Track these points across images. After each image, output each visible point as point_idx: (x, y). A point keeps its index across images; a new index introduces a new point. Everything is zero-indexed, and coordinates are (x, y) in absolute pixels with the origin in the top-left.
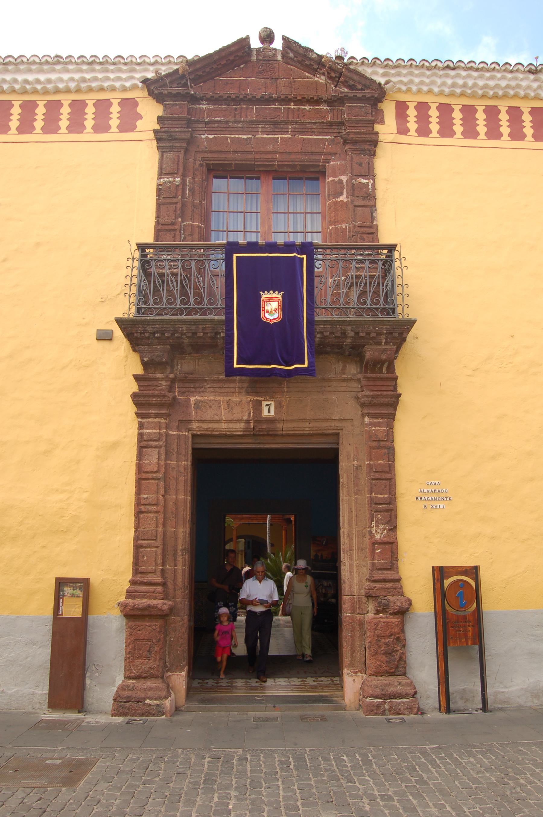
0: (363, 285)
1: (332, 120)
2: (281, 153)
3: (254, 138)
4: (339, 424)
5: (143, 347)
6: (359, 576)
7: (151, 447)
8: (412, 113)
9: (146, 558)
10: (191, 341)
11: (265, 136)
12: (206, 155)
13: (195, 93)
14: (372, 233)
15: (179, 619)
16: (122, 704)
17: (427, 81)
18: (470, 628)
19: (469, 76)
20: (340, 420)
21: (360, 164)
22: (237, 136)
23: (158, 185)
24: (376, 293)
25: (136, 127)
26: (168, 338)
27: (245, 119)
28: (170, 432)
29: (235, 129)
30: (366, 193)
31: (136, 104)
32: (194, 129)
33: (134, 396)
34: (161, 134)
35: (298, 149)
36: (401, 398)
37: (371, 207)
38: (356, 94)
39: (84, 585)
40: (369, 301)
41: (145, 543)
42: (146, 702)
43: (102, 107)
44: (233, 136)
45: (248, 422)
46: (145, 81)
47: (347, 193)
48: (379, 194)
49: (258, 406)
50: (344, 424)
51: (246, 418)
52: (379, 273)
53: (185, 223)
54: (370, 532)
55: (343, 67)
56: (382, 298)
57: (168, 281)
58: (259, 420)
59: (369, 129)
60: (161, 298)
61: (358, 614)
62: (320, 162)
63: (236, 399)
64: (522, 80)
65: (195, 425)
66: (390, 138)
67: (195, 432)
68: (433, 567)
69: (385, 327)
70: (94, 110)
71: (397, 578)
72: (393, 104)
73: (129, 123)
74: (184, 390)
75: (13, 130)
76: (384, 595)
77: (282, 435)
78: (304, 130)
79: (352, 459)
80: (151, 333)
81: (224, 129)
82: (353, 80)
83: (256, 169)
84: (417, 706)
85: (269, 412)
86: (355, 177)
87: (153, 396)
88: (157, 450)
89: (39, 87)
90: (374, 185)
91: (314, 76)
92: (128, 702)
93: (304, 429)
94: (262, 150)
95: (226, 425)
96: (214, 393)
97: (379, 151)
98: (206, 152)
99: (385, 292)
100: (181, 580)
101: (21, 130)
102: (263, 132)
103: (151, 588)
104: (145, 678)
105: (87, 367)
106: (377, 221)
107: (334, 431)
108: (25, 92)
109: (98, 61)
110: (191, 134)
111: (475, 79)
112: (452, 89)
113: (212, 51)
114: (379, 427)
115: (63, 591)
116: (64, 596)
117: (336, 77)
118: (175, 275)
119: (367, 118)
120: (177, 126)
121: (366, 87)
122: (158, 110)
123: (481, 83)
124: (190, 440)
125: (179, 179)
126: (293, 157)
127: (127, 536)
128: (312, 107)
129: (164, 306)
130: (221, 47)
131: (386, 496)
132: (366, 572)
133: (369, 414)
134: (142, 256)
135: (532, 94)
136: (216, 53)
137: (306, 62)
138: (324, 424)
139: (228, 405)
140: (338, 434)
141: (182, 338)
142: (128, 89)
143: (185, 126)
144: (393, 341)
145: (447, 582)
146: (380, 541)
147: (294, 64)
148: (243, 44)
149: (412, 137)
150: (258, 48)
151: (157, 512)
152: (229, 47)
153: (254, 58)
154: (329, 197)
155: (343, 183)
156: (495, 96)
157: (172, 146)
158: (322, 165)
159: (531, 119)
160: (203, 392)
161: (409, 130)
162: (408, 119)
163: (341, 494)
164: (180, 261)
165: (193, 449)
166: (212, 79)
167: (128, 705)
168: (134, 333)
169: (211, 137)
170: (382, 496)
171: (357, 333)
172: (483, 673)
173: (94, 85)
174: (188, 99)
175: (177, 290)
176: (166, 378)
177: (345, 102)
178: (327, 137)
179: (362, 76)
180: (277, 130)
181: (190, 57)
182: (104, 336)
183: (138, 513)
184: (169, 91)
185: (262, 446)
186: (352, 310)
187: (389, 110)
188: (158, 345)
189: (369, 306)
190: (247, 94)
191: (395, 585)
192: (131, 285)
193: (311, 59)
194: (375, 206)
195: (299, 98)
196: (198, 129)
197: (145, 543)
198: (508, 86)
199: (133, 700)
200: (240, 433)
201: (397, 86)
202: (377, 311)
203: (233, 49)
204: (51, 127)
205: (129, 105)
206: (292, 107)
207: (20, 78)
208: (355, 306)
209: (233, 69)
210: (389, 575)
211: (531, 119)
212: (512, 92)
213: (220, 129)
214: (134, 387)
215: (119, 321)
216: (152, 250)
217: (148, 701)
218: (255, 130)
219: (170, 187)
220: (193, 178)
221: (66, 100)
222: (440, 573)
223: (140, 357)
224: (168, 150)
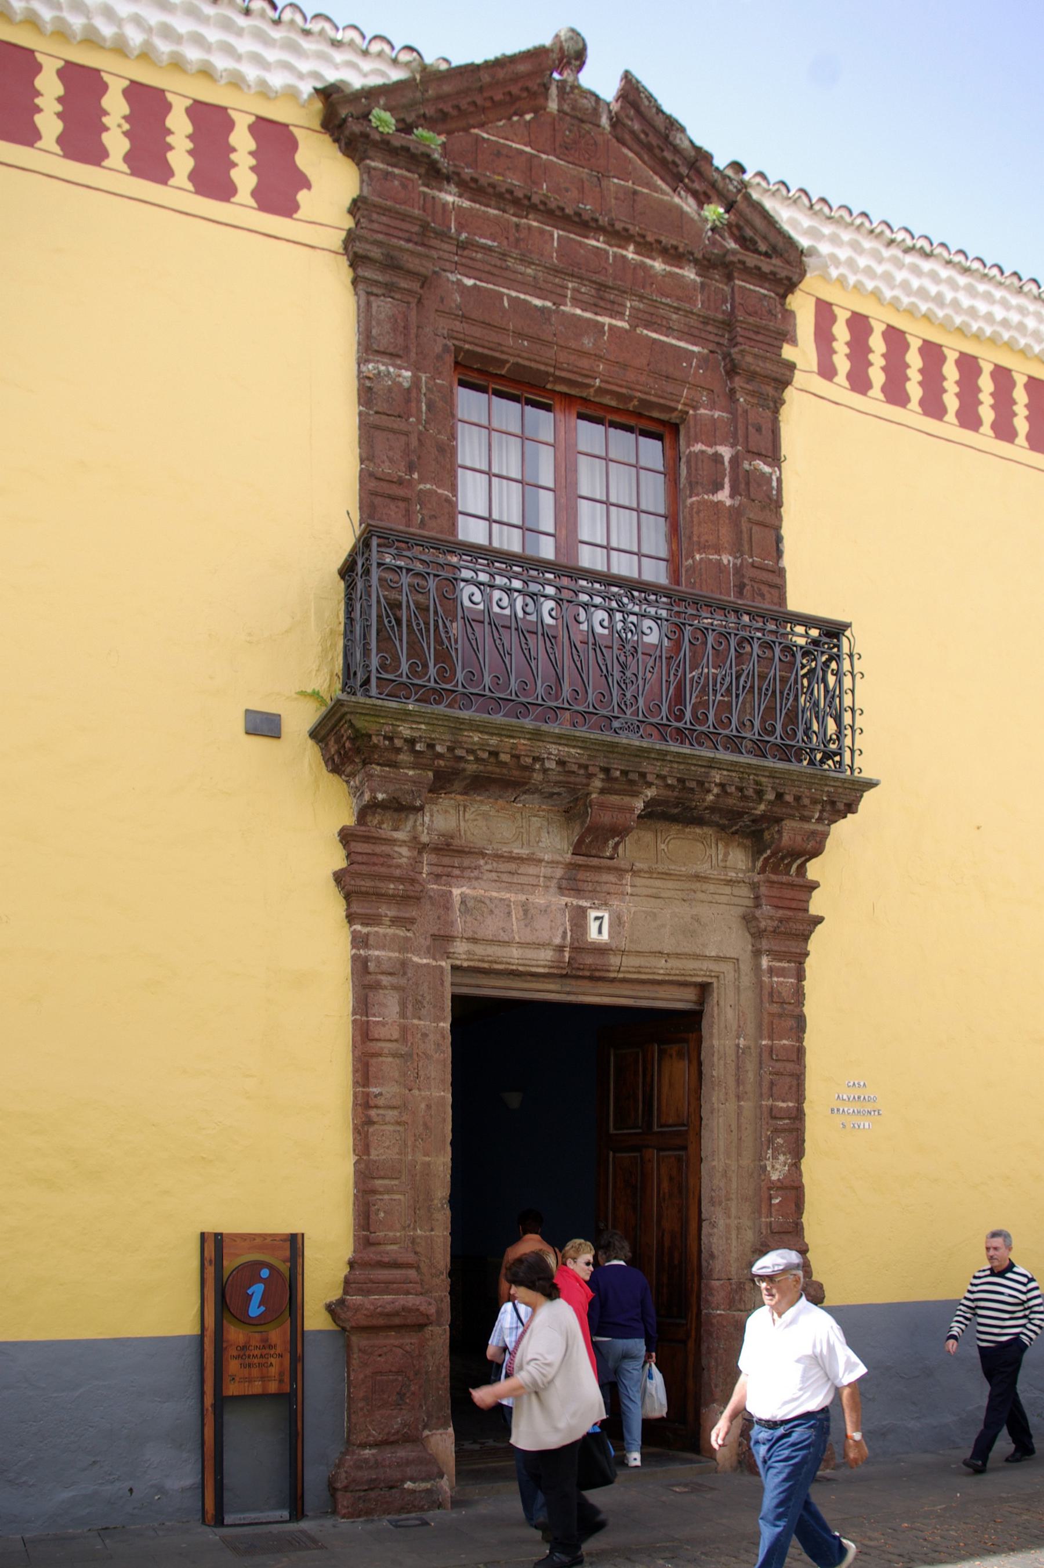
4: (715, 967)
5: (378, 768)
9: (382, 1215)
11: (578, 312)
16: (362, 1494)
20: (718, 959)
22: (522, 296)
28: (416, 959)
33: (339, 877)
42: (406, 1486)
45: (560, 949)
49: (579, 918)
51: (557, 941)
56: (689, 708)
58: (580, 947)
63: (539, 899)
67: (458, 963)
69: (826, 789)
73: (280, 191)
74: (439, 870)
79: (734, 1033)
80: (406, 740)
82: (753, 227)
83: (549, 386)
85: (600, 932)
91: (674, 190)
92: (372, 1489)
93: (656, 970)
95: (520, 951)
102: (576, 302)
104: (392, 1443)
113: (479, 60)
120: (400, 234)
128: (668, 268)
131: (791, 1104)
133: (769, 952)
136: (488, 65)
138: (691, 965)
139: (526, 912)
141: (467, 761)
143: (415, 238)
146: (779, 1184)
147: (636, 147)
155: (723, 463)
157: (392, 284)
158: (681, 411)
160: (477, 878)
164: (404, 571)
165: (455, 998)
167: (372, 1494)
169: (470, 282)
170: (784, 1105)
171: (780, 796)
173: (193, 54)
174: (422, 171)
177: (736, 274)
178: (696, 349)
180: (602, 304)
182: (264, 726)
193: (676, 150)
199: (382, 1485)
213: (488, 268)
217: (408, 1485)
224: (379, 291)
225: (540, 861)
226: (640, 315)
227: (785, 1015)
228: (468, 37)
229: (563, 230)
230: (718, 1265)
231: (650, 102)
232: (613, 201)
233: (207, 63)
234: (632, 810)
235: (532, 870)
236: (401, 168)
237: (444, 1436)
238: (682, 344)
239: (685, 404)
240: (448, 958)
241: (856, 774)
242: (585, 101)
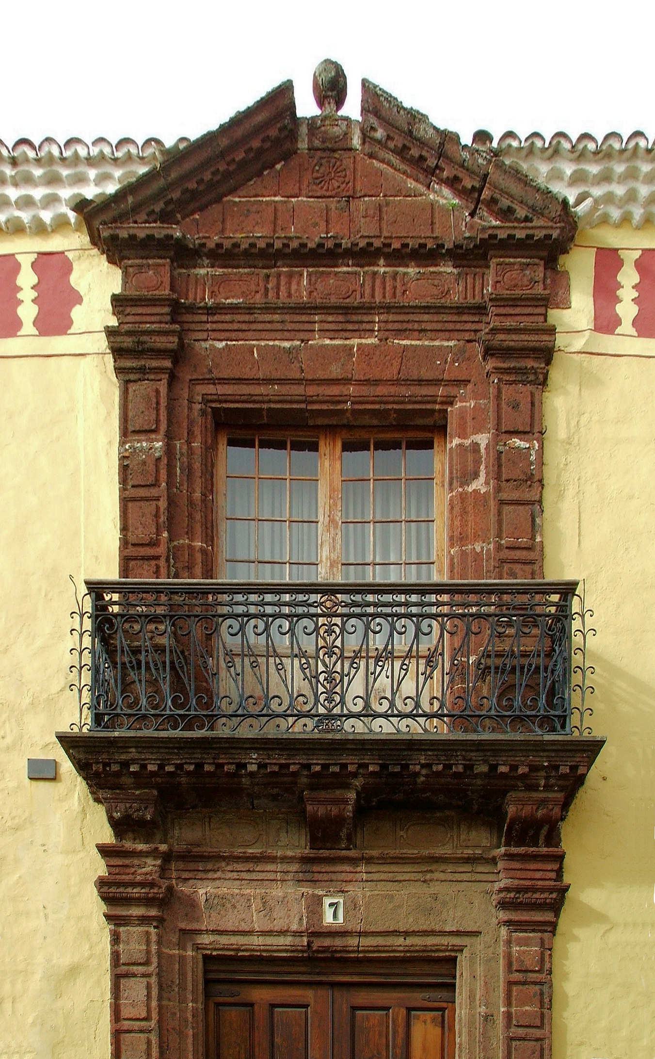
1: (461, 301)
3: (306, 348)
7: (134, 975)
10: (194, 780)
11: (328, 342)
13: (184, 236)
14: (531, 562)
20: (457, 933)
22: (271, 343)
23: (122, 458)
25: (71, 322)
26: (153, 774)
27: (287, 301)
30: (525, 473)
31: (67, 267)
32: (186, 326)
33: (102, 883)
35: (390, 373)
36: (569, 894)
37: (532, 503)
38: (512, 232)
44: (263, 343)
46: (81, 206)
47: (487, 474)
50: (465, 941)
53: (175, 543)
57: (147, 663)
59: (535, 318)
60: (163, 699)
63: (277, 892)
66: (578, 343)
67: (209, 952)
77: (357, 960)
81: (244, 327)
83: (311, 423)
86: (504, 436)
87: (134, 885)
88: (145, 980)
91: (428, 187)
94: (320, 375)
96: (238, 882)
97: (555, 374)
99: (549, 683)
105: (16, 829)
106: (542, 535)
110: (181, 339)
113: (214, 127)
114: (527, 945)
118: (160, 649)
119: (534, 292)
124: (201, 964)
125: (161, 443)
126: (381, 390)
129: (143, 712)
130: (232, 114)
136: (224, 129)
137: (412, 152)
142: (49, 229)
144: (560, 782)
150: (313, 118)
153: (303, 145)
154: (451, 484)
164: (168, 618)
168: (91, 764)
179: (524, 180)
182: (42, 772)
184: (132, 232)
186: (487, 721)
187: (580, 266)
188: (136, 789)
190: (290, 238)
193: (422, 143)
194: (540, 502)
196: (193, 326)
203: (260, 118)
205: (54, 267)
206: (382, 270)
208: (493, 712)
213: (236, 326)
214: (100, 868)
215: (66, 740)
216: (116, 597)
218: (307, 327)
219: (144, 463)
223: (107, 812)
225: (275, 858)
226: (390, 326)
228: (195, 108)
229: (310, 266)
231: (390, 102)
234: (345, 801)
235: (270, 867)
236: (153, 258)
238: (437, 343)
241: (585, 734)
242: (336, 129)
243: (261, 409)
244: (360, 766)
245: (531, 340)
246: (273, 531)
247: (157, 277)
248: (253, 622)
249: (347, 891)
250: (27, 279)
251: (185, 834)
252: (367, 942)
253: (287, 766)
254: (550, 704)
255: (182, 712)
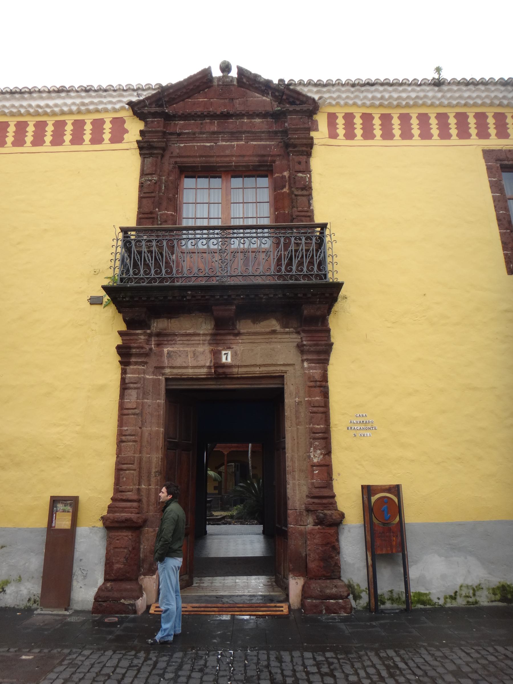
0: (300, 256)
2: (236, 156)
6: (300, 493)
8: (340, 121)
9: (125, 479)
11: (224, 143)
12: (178, 160)
14: (309, 216)
15: (151, 530)
17: (352, 96)
18: (394, 538)
19: (385, 90)
20: (284, 365)
21: (299, 163)
22: (202, 144)
24: (311, 263)
25: (123, 139)
28: (147, 377)
29: (201, 139)
31: (124, 122)
32: (168, 139)
33: (118, 348)
34: (142, 144)
39: (73, 502)
40: (305, 269)
41: (125, 467)
43: (98, 125)
44: (199, 144)
45: (209, 367)
46: (130, 104)
48: (315, 185)
49: (216, 354)
52: (313, 246)
54: (309, 456)
55: (285, 88)
56: (316, 266)
58: (218, 365)
60: (139, 271)
61: (300, 525)
62: (267, 162)
63: (200, 349)
64: (428, 91)
65: (167, 371)
67: (168, 376)
68: (362, 486)
70: (91, 127)
71: (331, 495)
72: (326, 116)
73: (118, 136)
75: (28, 143)
76: (321, 509)
77: (238, 378)
78: (255, 138)
79: (294, 396)
83: (218, 170)
84: (350, 606)
85: (226, 359)
89: (48, 110)
90: (310, 178)
94: (222, 154)
95: (192, 370)
98: (177, 157)
99: (318, 261)
100: (153, 497)
101: (34, 143)
102: (223, 140)
103: (129, 504)
107: (280, 374)
108: (37, 114)
109: (93, 89)
110: (166, 143)
111: (390, 92)
112: (372, 101)
115: (56, 507)
116: (57, 511)
117: (279, 95)
121: (302, 103)
122: (140, 125)
123: (395, 95)
124: (164, 382)
126: (246, 159)
127: (109, 462)
130: (186, 76)
131: (322, 426)
132: (305, 490)
133: (307, 360)
134: (124, 237)
135: (437, 103)
136: (185, 80)
139: (194, 354)
140: (283, 376)
145: (374, 499)
146: (318, 464)
148: (206, 74)
149: (341, 140)
151: (135, 441)
152: (195, 75)
156: (407, 106)
157: (152, 153)
159: (437, 122)
160: (174, 344)
161: (338, 135)
162: (338, 126)
163: (286, 425)
166: (183, 100)
170: (319, 427)
172: (406, 578)
173: (91, 107)
175: (152, 263)
176: (145, 334)
178: (273, 143)
181: (164, 84)
182: (95, 301)
183: (120, 442)
185: (222, 387)
187: (322, 120)
189: (305, 273)
190: (210, 111)
191: (331, 500)
192: (116, 260)
193: (259, 83)
195: (250, 113)
197: (125, 467)
198: (417, 97)
200: (203, 377)
201: (328, 101)
202: (312, 277)
204: (58, 140)
205: (118, 124)
207: (34, 103)
209: (199, 92)
210: (325, 492)
211: (437, 122)
212: (421, 102)
213: (189, 139)
216: (133, 233)
217: (122, 601)
220: (168, 177)
221: (70, 120)
222: (368, 491)
227: (321, 386)
228: (174, 72)
230: (290, 503)
232: (238, 106)
233: (97, 108)
235: (197, 338)
237: (151, 579)
239: (270, 162)
240: (163, 375)
243: (198, 166)
244: (237, 295)
245: (305, 141)
246: (243, 207)
247: (158, 124)
248: (190, 241)
249: (233, 348)
250: (12, 129)
251: (158, 325)
252: (242, 370)
253: (204, 296)
254: (319, 269)
255: (147, 276)
